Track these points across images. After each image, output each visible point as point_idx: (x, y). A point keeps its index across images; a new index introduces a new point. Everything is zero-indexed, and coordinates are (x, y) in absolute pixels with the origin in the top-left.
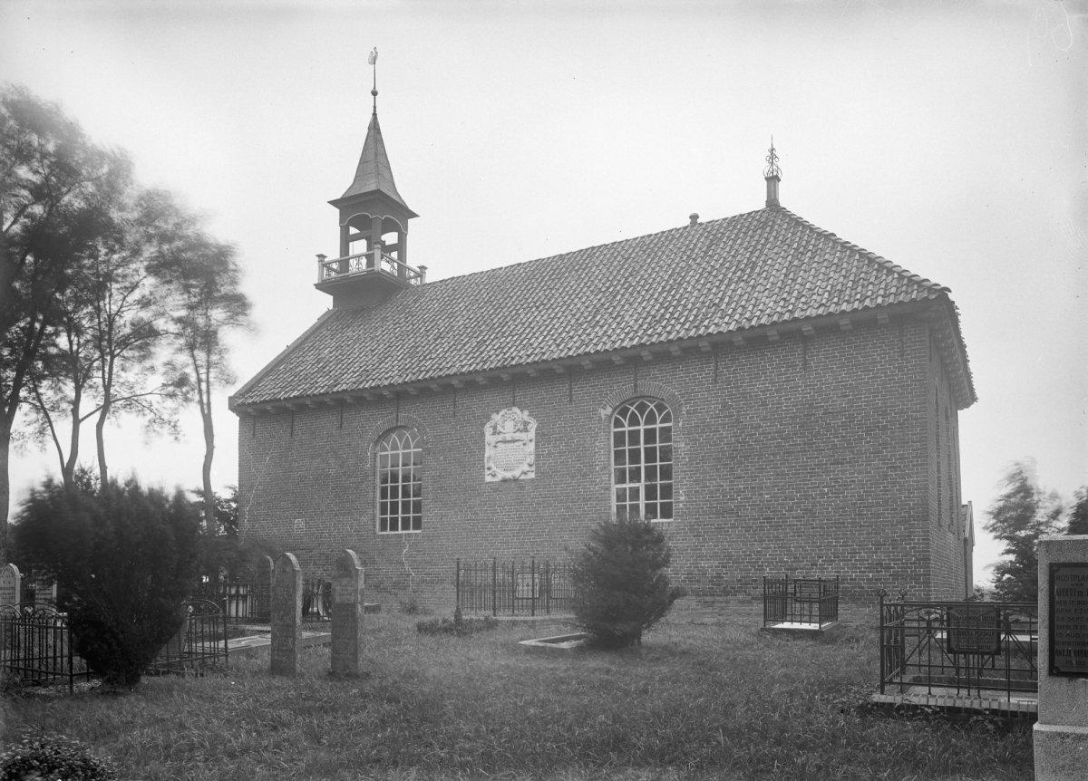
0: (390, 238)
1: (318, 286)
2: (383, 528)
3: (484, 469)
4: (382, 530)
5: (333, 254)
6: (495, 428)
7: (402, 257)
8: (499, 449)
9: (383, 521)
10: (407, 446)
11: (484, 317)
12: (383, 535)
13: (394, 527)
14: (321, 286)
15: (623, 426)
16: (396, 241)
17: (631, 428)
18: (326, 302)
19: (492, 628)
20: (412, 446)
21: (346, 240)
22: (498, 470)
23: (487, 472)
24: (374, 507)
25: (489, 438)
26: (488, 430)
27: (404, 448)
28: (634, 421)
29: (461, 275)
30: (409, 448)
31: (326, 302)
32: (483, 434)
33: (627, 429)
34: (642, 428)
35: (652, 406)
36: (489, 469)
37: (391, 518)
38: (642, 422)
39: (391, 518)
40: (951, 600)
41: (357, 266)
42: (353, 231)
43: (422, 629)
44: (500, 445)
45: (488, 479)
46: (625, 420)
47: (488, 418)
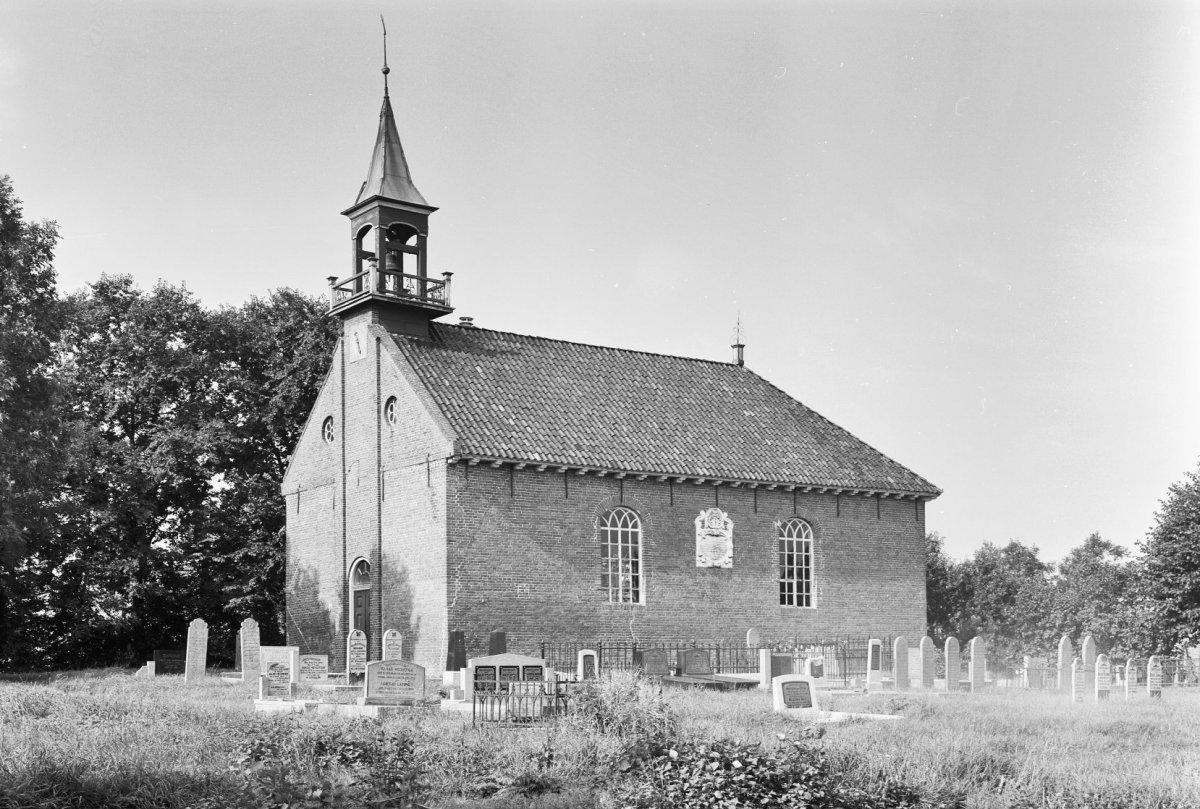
45: (730, 566)
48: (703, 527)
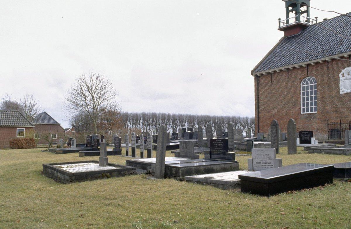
0: (304, 9)
1: (279, 29)
2: (304, 111)
3: (339, 89)
4: (303, 112)
5: (284, 18)
6: (343, 75)
7: (308, 15)
8: (345, 82)
9: (304, 109)
10: (311, 83)
11: (318, 37)
12: (304, 114)
13: (308, 111)
14: (280, 29)
15: (304, 85)
16: (306, 9)
17: (308, 85)
18: (282, 34)
19: (53, 174)
20: (313, 83)
21: (288, 12)
22: (344, 90)
23: (341, 90)
24: (300, 105)
25: (341, 78)
26: (340, 75)
27: (310, 84)
28: (307, 83)
29: (336, 16)
30: (312, 83)
31: (282, 34)
32: (339, 77)
33: (305, 86)
34: (309, 85)
35: (311, 79)
36: (341, 89)
37: (306, 108)
38: (309, 83)
39: (306, 108)
40: (283, 163)
41: (292, 21)
42: (290, 8)
43: (307, 148)
44: (346, 80)
45: (341, 93)
46: (309, 81)
47: (341, 71)
48: (343, 76)
